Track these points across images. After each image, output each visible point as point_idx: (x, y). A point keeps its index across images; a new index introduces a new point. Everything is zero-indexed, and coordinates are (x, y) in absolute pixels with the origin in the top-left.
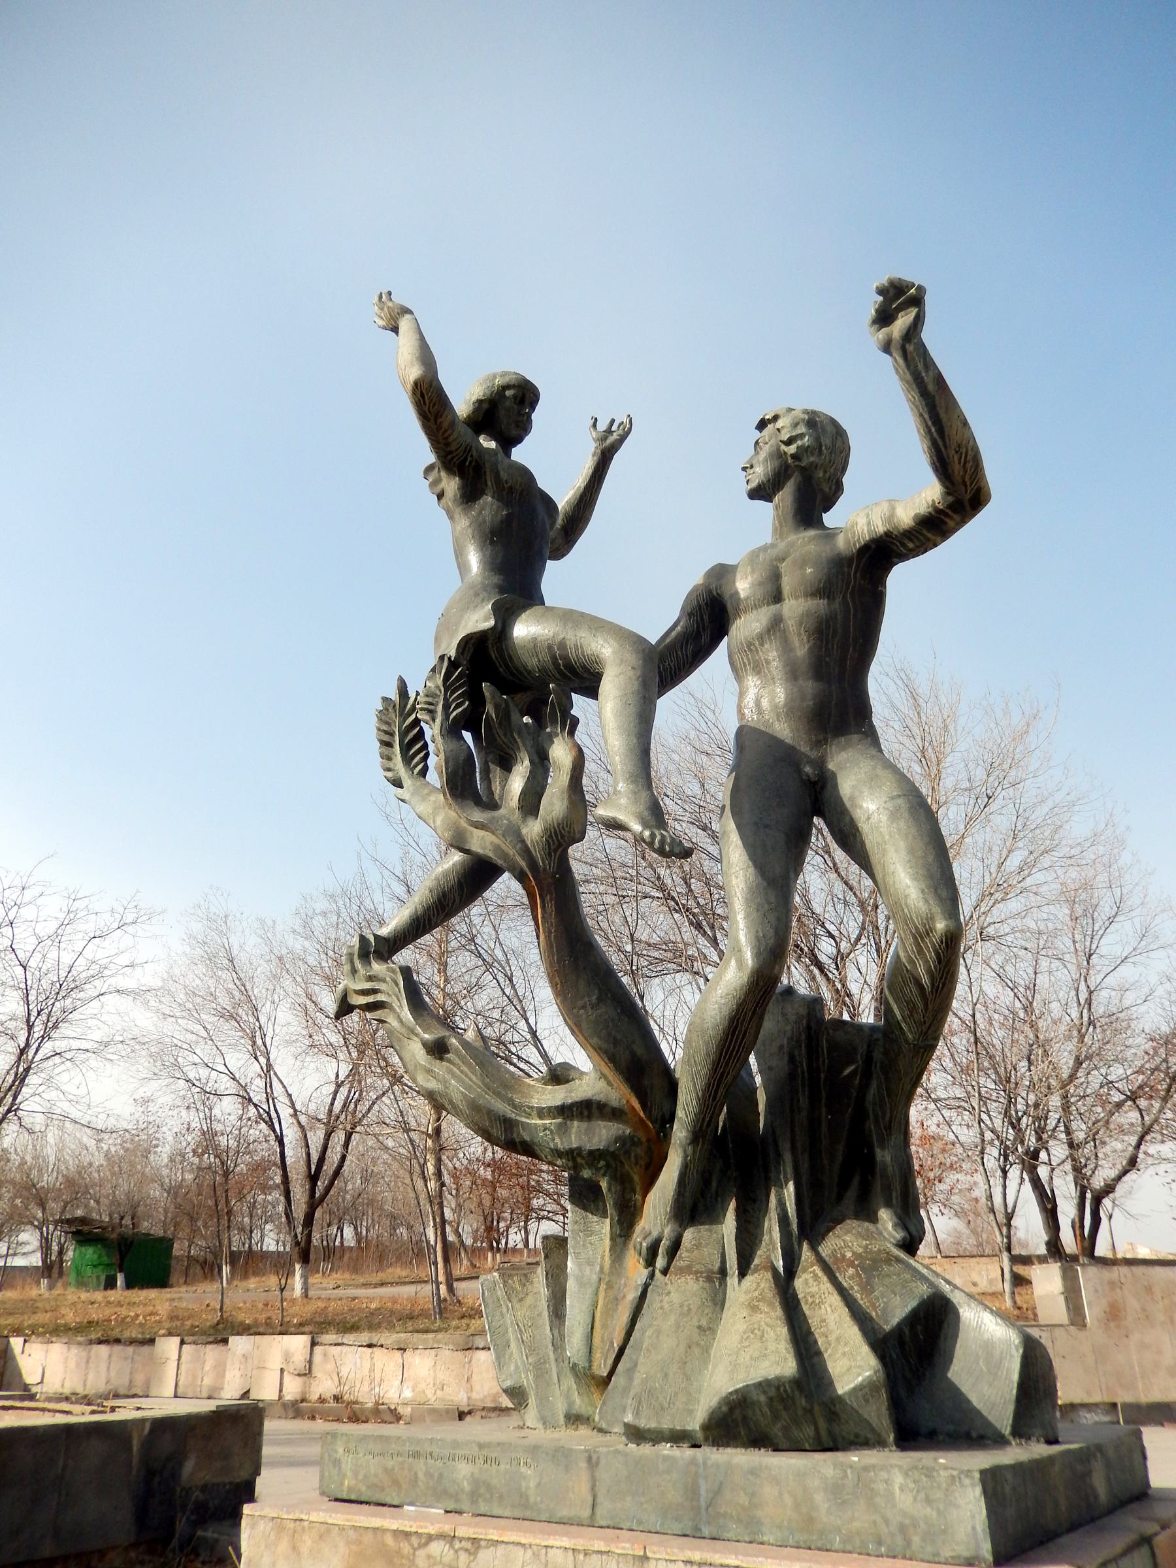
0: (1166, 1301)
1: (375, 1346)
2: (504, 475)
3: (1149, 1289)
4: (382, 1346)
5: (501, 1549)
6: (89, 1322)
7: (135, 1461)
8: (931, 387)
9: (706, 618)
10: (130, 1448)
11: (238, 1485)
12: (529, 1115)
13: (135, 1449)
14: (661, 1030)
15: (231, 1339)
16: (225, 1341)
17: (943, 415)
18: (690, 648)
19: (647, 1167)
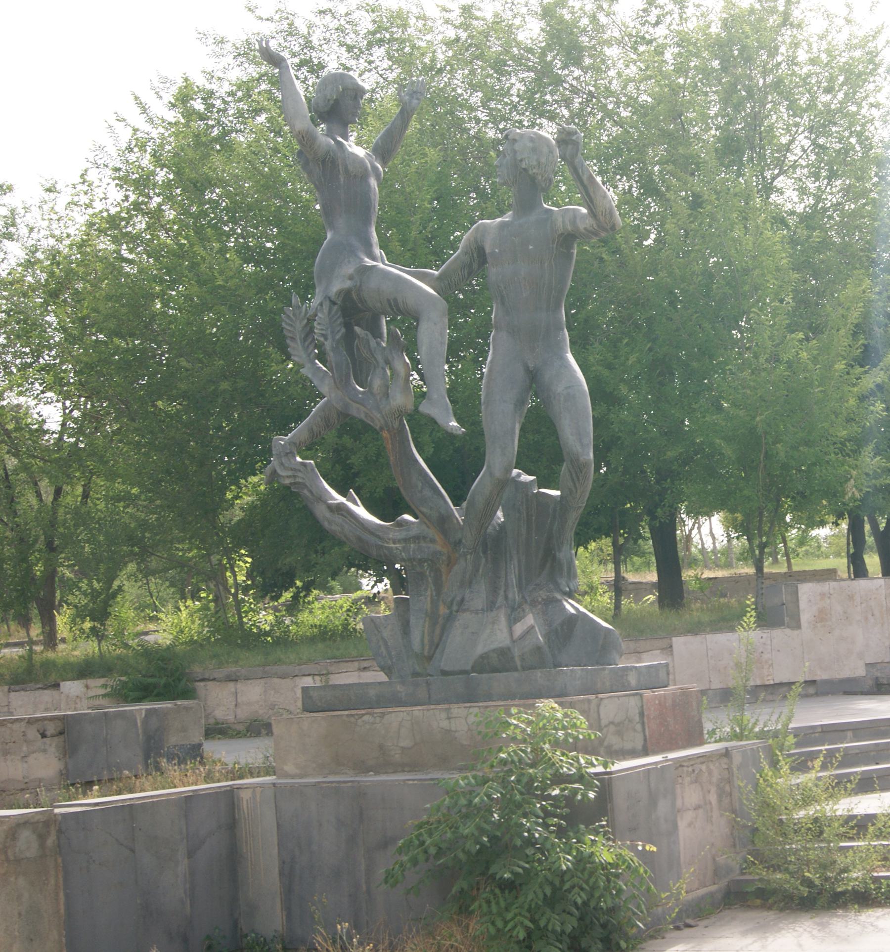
0: (863, 605)
1: (208, 680)
2: (351, 168)
3: (851, 597)
4: (214, 679)
5: (393, 715)
6: (477, 614)
7: (140, 731)
8: (586, 182)
9: (475, 255)
10: (136, 724)
11: (194, 745)
12: (388, 543)
13: (139, 724)
14: (428, 710)
15: (62, 684)
16: (56, 686)
17: (592, 194)
18: (466, 272)
19: (448, 565)
